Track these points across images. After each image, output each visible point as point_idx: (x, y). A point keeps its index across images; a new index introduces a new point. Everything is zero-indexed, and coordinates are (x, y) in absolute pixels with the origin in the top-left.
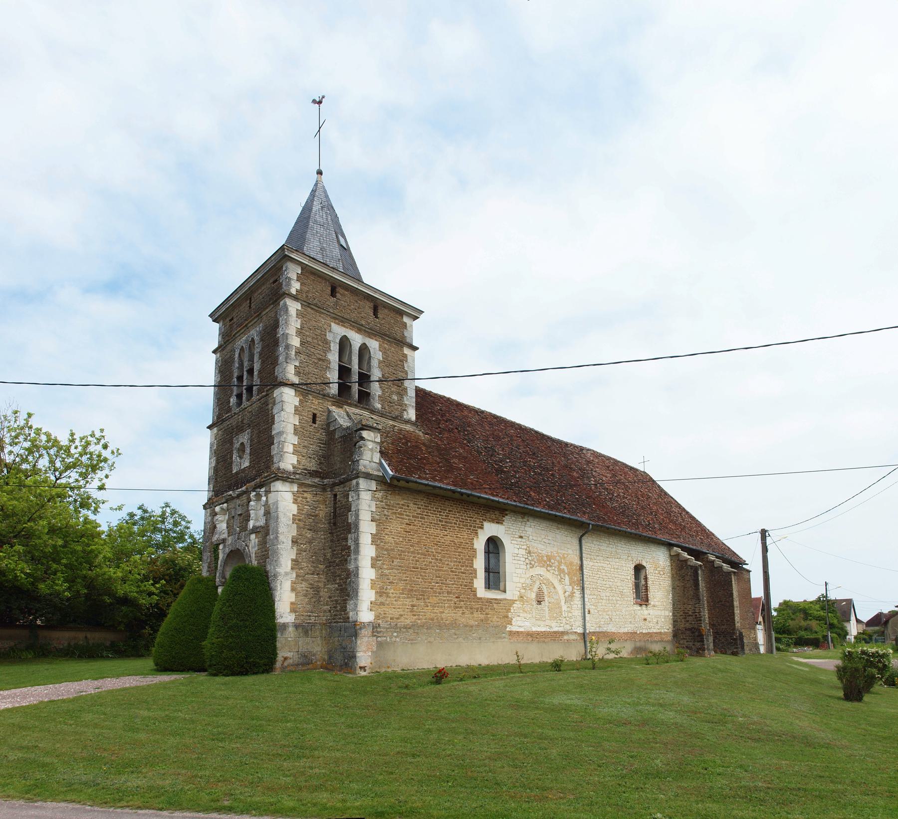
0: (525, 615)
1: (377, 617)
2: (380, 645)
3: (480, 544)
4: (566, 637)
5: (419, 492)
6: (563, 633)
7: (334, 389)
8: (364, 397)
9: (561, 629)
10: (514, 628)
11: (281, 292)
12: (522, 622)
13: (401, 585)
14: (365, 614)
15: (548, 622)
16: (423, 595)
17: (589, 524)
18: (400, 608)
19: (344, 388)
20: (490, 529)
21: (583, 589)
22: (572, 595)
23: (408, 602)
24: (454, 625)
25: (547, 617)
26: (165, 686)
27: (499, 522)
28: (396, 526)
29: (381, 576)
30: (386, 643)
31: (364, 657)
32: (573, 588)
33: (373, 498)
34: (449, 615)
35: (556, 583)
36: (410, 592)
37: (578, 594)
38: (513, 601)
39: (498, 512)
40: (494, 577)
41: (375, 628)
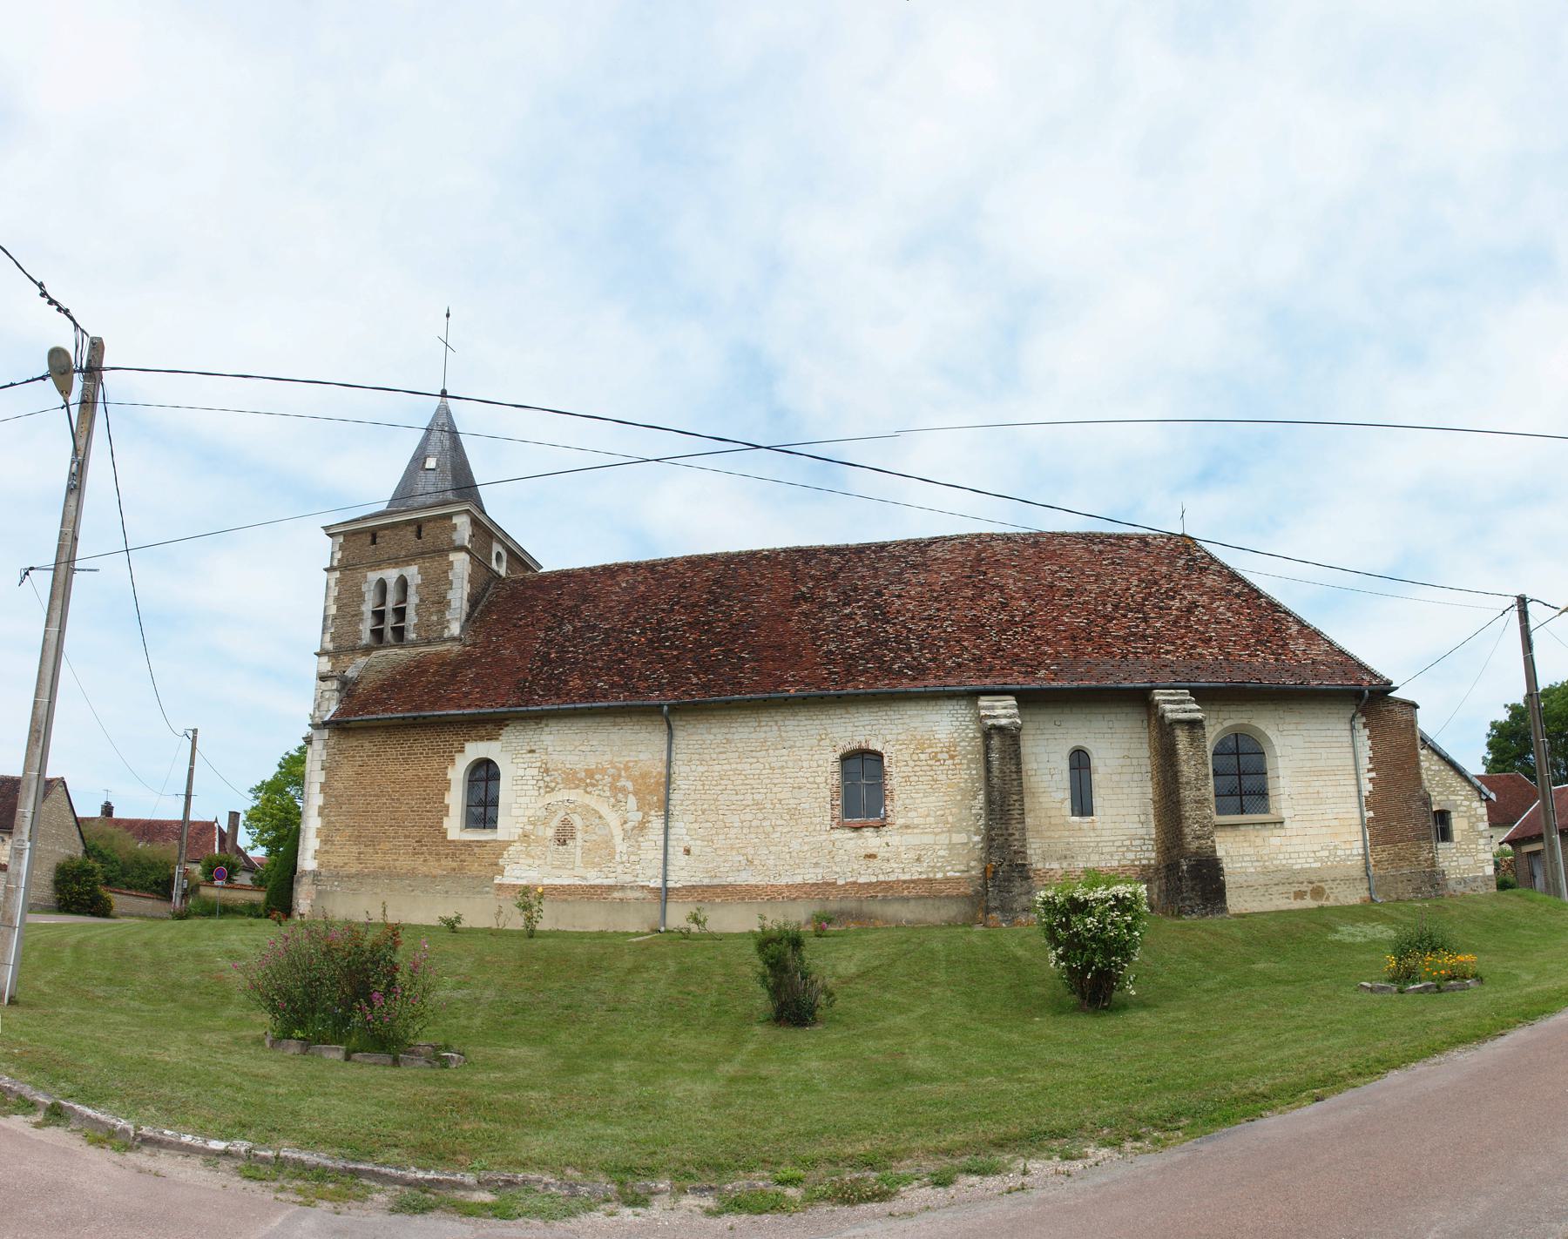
0: (530, 861)
1: (321, 865)
2: (319, 893)
3: (457, 773)
4: (616, 895)
5: (375, 728)
6: (610, 888)
7: (366, 637)
8: (399, 632)
9: (611, 882)
10: (507, 881)
11: (337, 574)
12: (519, 871)
13: (348, 831)
14: (307, 861)
15: (580, 871)
16: (372, 842)
17: (661, 706)
18: (346, 856)
19: (378, 634)
20: (476, 750)
21: (667, 816)
22: (642, 826)
23: (355, 849)
24: (412, 874)
25: (578, 861)
26: (83, 928)
27: (491, 738)
28: (347, 770)
29: (328, 824)
30: (326, 892)
31: (304, 901)
32: (646, 814)
33: (326, 746)
34: (404, 863)
35: (605, 810)
36: (357, 839)
37: (657, 824)
38: (509, 843)
39: (489, 725)
40: (483, 810)
41: (316, 875)
